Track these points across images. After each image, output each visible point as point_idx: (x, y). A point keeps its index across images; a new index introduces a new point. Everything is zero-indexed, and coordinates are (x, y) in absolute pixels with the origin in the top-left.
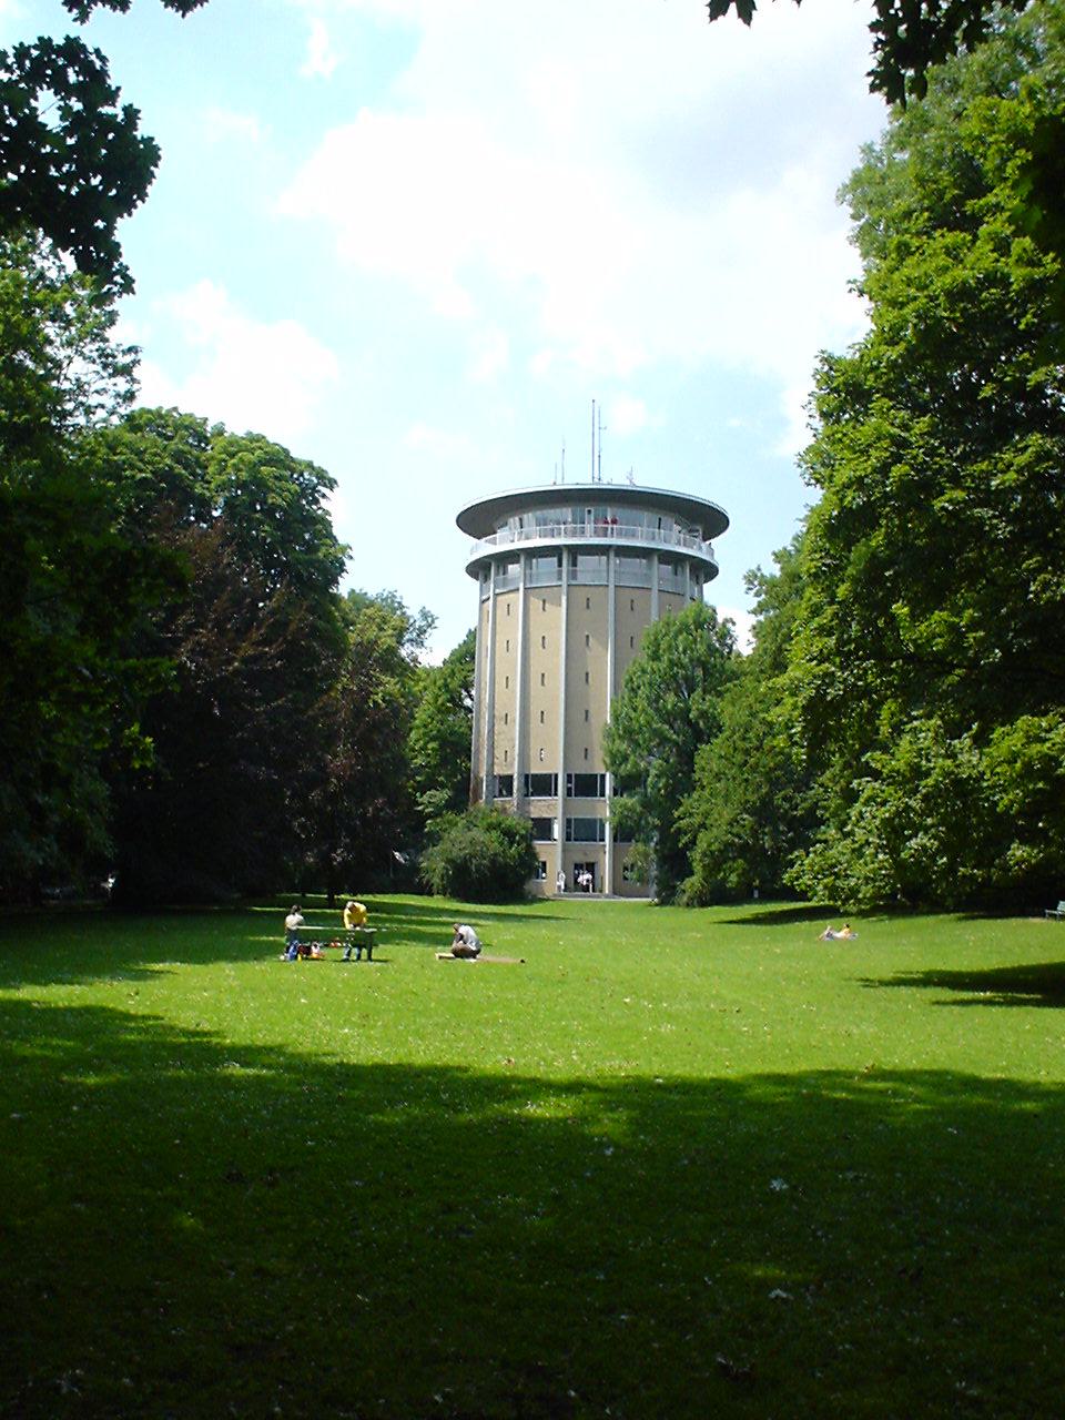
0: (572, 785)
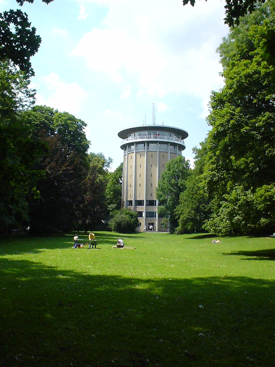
0: (148, 203)
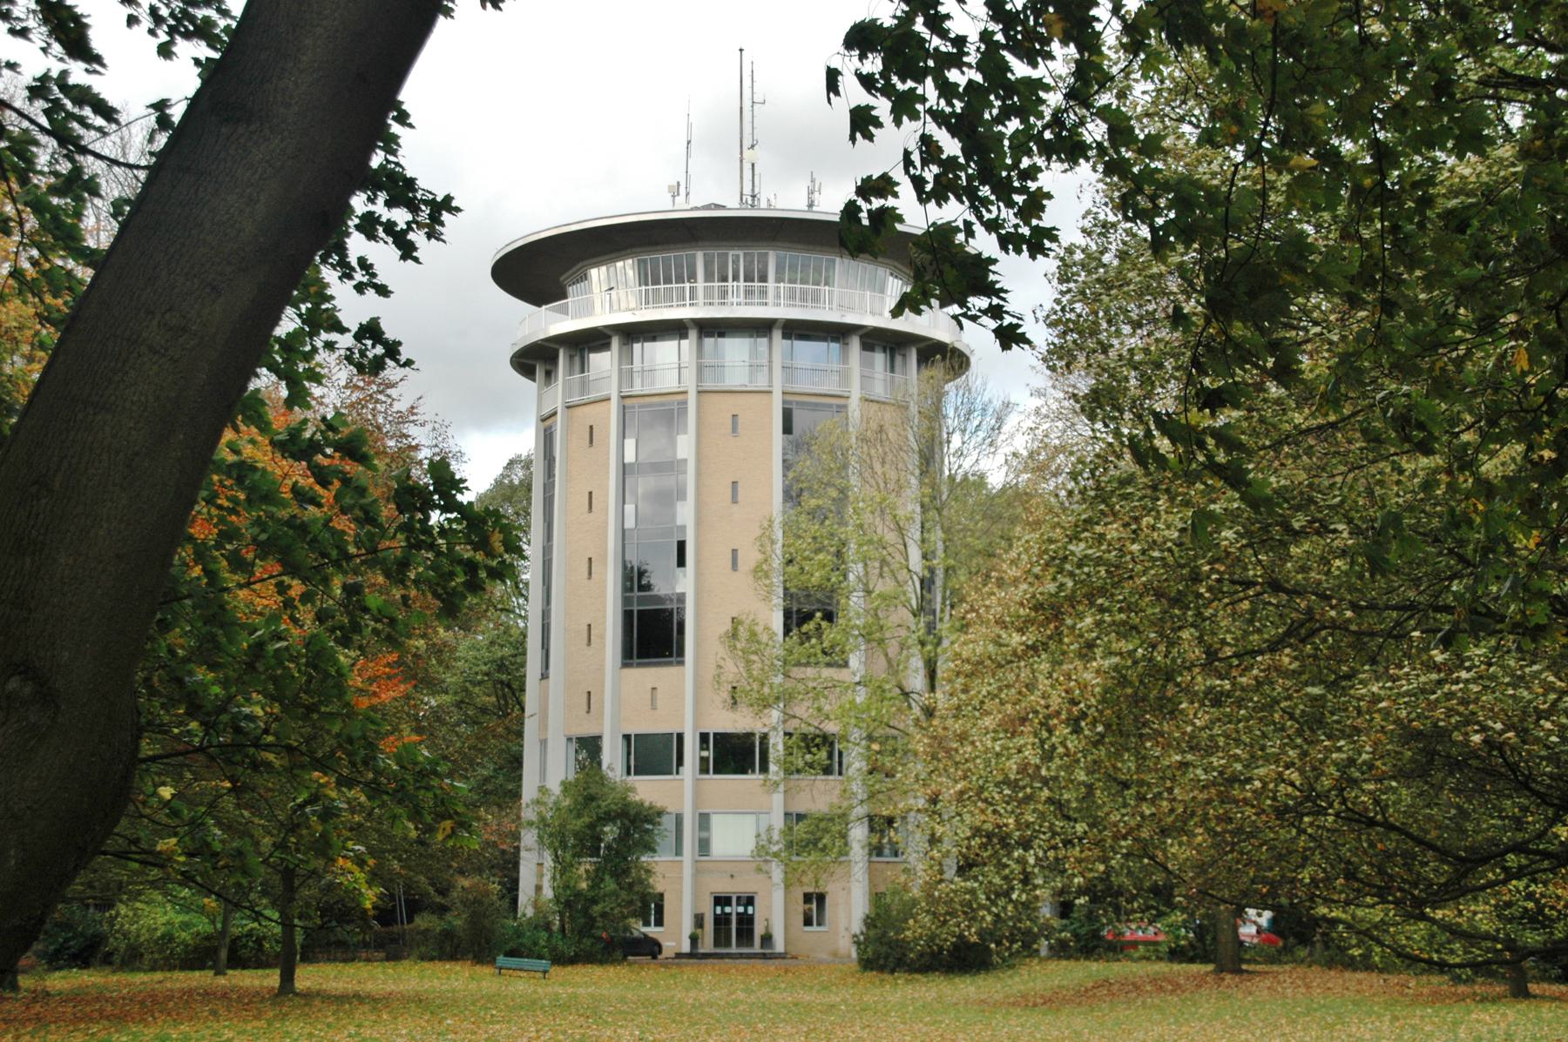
0: (709, 754)
